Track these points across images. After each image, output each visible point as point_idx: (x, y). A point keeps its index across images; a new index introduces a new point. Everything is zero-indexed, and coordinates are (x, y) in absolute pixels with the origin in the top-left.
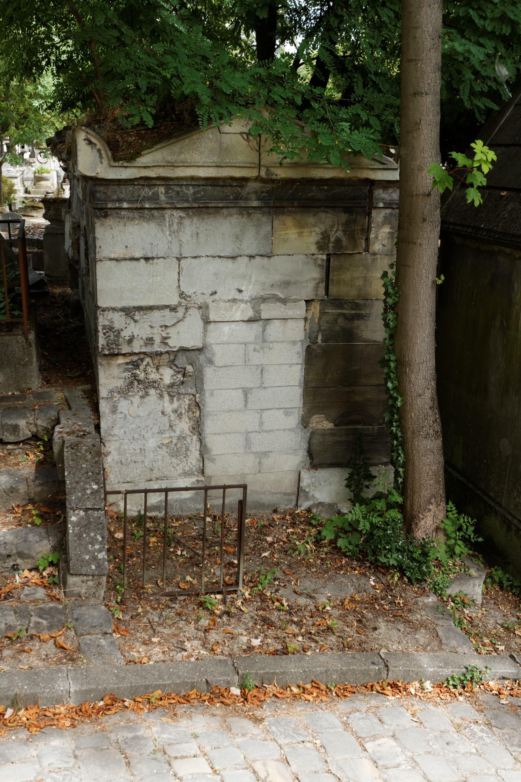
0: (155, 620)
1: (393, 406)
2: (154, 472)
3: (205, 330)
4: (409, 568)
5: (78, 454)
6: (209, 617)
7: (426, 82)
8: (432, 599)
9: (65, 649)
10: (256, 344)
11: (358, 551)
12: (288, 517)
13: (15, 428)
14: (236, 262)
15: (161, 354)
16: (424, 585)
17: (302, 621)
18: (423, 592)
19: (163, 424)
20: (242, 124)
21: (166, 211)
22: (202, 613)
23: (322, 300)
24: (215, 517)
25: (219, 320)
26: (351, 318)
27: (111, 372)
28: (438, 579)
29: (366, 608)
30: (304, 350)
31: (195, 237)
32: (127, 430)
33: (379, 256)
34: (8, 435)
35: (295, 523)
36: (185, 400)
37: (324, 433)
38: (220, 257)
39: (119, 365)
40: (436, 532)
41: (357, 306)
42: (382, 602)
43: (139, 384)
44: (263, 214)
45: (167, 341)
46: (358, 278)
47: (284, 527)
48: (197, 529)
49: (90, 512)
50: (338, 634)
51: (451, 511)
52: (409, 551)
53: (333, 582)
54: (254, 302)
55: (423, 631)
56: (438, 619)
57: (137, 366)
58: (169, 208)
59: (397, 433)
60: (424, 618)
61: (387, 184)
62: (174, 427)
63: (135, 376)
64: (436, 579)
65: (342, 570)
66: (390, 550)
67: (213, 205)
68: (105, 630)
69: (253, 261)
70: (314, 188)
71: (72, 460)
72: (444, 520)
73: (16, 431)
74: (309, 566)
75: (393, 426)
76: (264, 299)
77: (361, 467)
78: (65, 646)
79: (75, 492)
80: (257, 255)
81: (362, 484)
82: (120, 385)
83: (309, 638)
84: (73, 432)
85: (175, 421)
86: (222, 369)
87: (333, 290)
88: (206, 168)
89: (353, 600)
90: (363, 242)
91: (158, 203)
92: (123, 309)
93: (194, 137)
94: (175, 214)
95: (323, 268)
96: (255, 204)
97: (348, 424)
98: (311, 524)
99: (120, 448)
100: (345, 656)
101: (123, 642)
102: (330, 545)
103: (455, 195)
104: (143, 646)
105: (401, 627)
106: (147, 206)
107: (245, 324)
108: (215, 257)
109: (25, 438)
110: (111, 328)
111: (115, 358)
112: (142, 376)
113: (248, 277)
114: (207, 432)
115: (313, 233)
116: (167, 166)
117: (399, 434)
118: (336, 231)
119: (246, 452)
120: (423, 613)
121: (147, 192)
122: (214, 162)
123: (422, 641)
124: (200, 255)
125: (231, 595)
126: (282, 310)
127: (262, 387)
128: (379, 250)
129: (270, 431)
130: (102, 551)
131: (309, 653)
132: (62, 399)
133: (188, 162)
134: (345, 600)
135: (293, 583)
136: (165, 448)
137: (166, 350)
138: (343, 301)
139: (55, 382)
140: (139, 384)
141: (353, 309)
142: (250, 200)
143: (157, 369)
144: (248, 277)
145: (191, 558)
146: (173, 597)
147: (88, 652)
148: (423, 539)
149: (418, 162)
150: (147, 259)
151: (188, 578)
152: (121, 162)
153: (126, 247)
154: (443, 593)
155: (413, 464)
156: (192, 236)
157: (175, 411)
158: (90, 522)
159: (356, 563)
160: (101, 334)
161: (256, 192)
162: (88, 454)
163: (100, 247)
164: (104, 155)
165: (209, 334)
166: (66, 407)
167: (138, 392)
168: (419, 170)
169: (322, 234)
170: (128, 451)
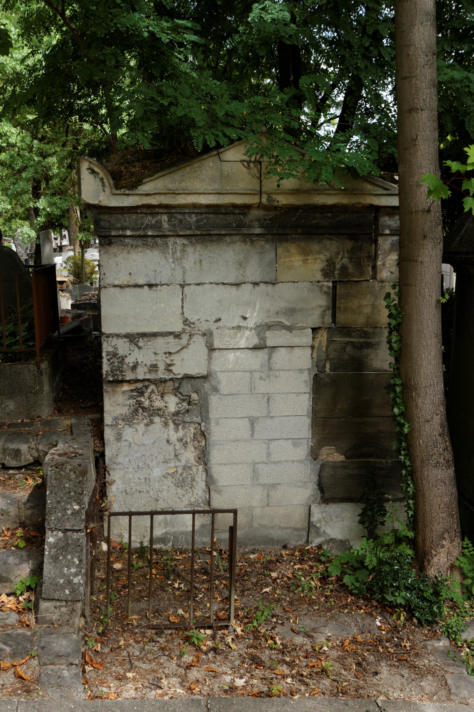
0: (135, 654)
1: (401, 433)
2: (159, 502)
3: (210, 358)
4: (419, 608)
5: (62, 473)
6: (194, 653)
7: (421, 98)
8: (443, 643)
9: (24, 679)
10: (262, 372)
11: (365, 589)
12: (297, 553)
13: (17, 453)
14: (240, 289)
15: (165, 381)
16: (436, 628)
17: (294, 662)
18: (435, 636)
19: (168, 453)
20: (242, 152)
21: (169, 239)
22: (187, 648)
23: (329, 328)
24: (221, 550)
25: (224, 347)
26: (360, 347)
27: (116, 399)
28: (452, 621)
29: (368, 650)
30: (312, 378)
31: (198, 264)
32: (131, 458)
33: (387, 283)
34: (10, 459)
35: (303, 560)
36: (190, 428)
37: (335, 466)
38: (223, 284)
39: (124, 392)
40: (451, 570)
41: (365, 334)
42: (387, 644)
43: (144, 411)
44: (267, 241)
45: (171, 368)
46: (366, 305)
47: (292, 564)
48: (200, 562)
49: (69, 533)
50: (333, 677)
51: (468, 548)
52: (420, 589)
53: (336, 621)
54: (260, 329)
55: (429, 677)
56: (449, 665)
57: (141, 393)
58: (172, 236)
59: (405, 462)
60: (433, 663)
61: (391, 211)
62: (179, 457)
63: (139, 403)
64: (449, 621)
65: (347, 608)
66: (398, 588)
67: (216, 232)
68: (71, 660)
69: (257, 288)
70: (318, 215)
71: (56, 479)
72: (459, 558)
73: (18, 456)
74: (312, 603)
75: (401, 455)
76: (269, 327)
77: (375, 503)
78: (23, 676)
79: (55, 512)
80: (262, 282)
81: (377, 521)
82: (124, 413)
83: (300, 681)
84: (65, 454)
85: (180, 450)
86: (227, 397)
87: (341, 317)
88: (207, 196)
89: (354, 641)
90: (370, 269)
91: (161, 231)
92: (127, 336)
93: (195, 165)
94: (178, 242)
95: (329, 295)
96: (258, 231)
97: (360, 456)
98: (320, 561)
99: (124, 476)
100: (336, 702)
101: (95, 676)
102: (337, 583)
103: (468, 227)
104: (115, 681)
105: (405, 672)
106: (150, 233)
107: (250, 351)
108: (218, 284)
109: (27, 463)
110: (115, 355)
111: (119, 385)
112: (147, 403)
113: (252, 305)
114: (213, 462)
115: (318, 260)
116: (168, 193)
117: (408, 463)
118: (342, 259)
119: (253, 483)
120: (432, 658)
121: (150, 220)
122: (215, 190)
123: (428, 689)
124: (203, 282)
125: (223, 631)
126: (288, 337)
127: (269, 416)
128: (387, 277)
129: (278, 462)
130: (78, 575)
131: (296, 697)
132: (67, 425)
133: (189, 190)
134: (345, 640)
135: (291, 621)
136: (170, 478)
137: (170, 377)
138: (350, 329)
139: (67, 411)
140: (144, 411)
141: (361, 337)
142: (253, 227)
143: (162, 397)
144: (252, 305)
145: (188, 591)
146: (159, 630)
147: (47, 683)
148: (436, 577)
149: (416, 179)
150: (151, 286)
151: (180, 611)
152: (123, 190)
153: (130, 274)
154: (457, 637)
155: (424, 495)
156: (195, 263)
157: (180, 440)
158: (68, 544)
159: (362, 601)
160: (105, 361)
161: (258, 220)
162: (72, 473)
163: (104, 274)
164: (106, 184)
165: (213, 361)
166: (69, 432)
167: (143, 419)
168: (417, 186)
169: (327, 261)
170: (132, 480)
